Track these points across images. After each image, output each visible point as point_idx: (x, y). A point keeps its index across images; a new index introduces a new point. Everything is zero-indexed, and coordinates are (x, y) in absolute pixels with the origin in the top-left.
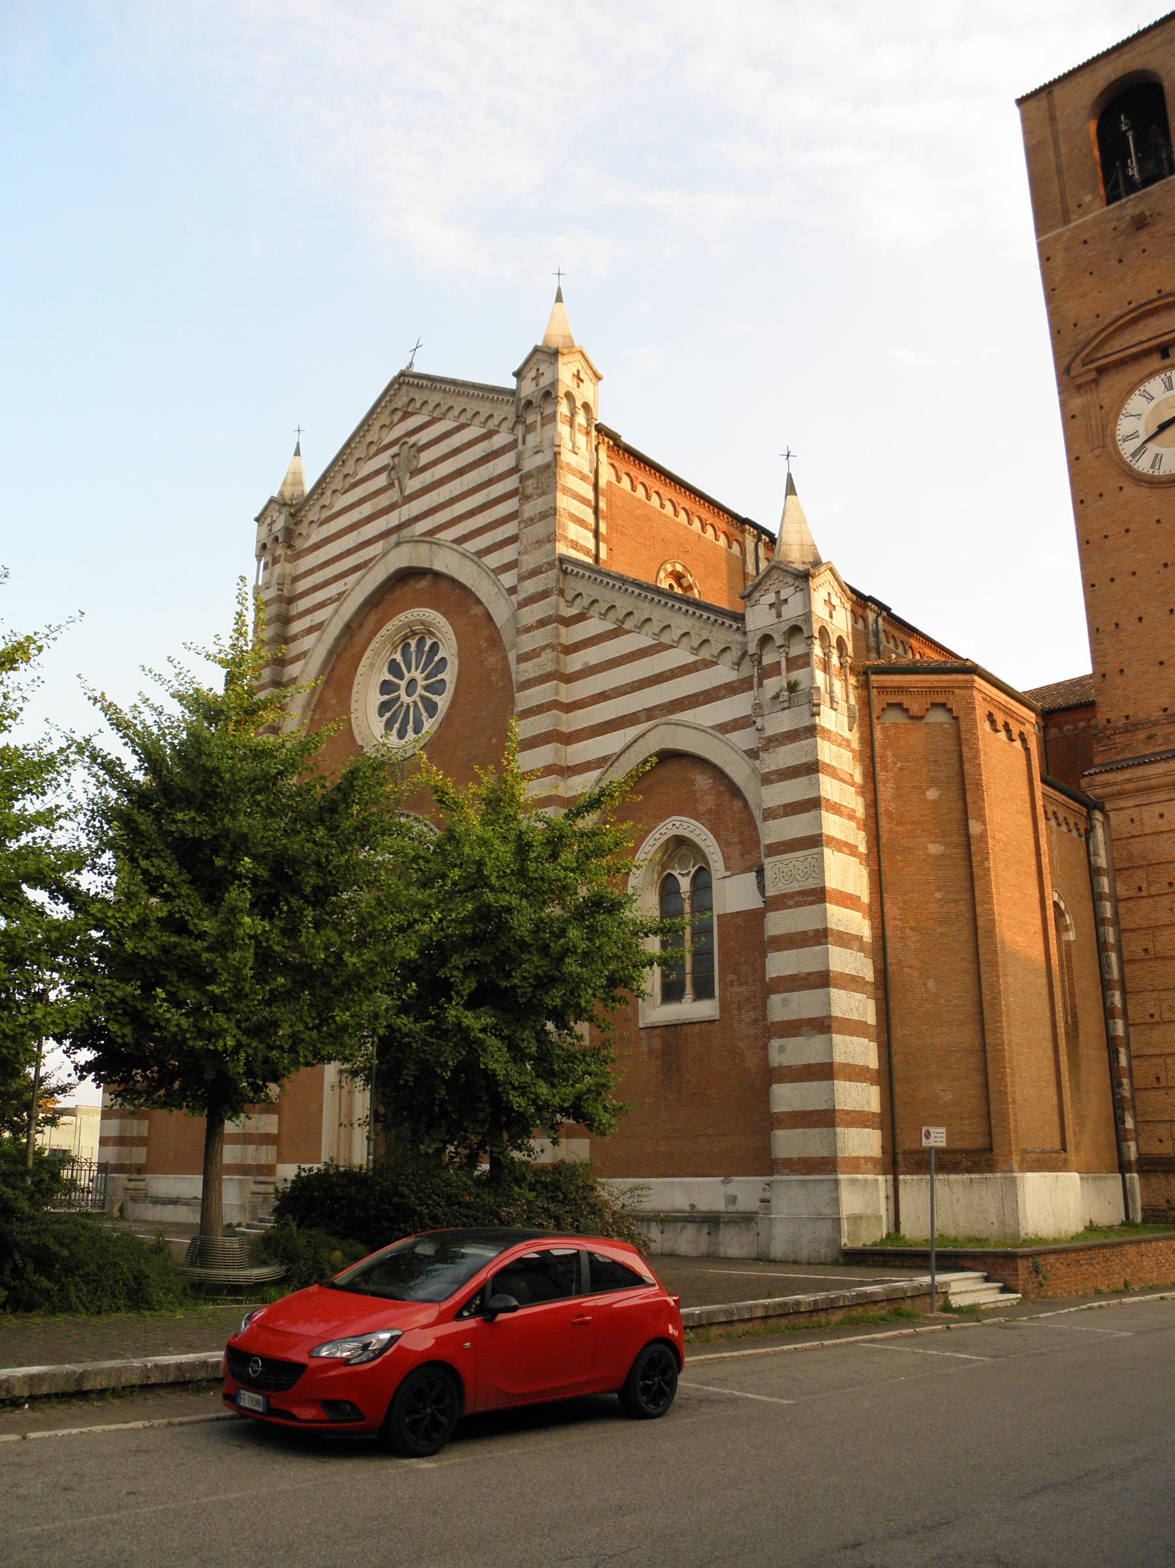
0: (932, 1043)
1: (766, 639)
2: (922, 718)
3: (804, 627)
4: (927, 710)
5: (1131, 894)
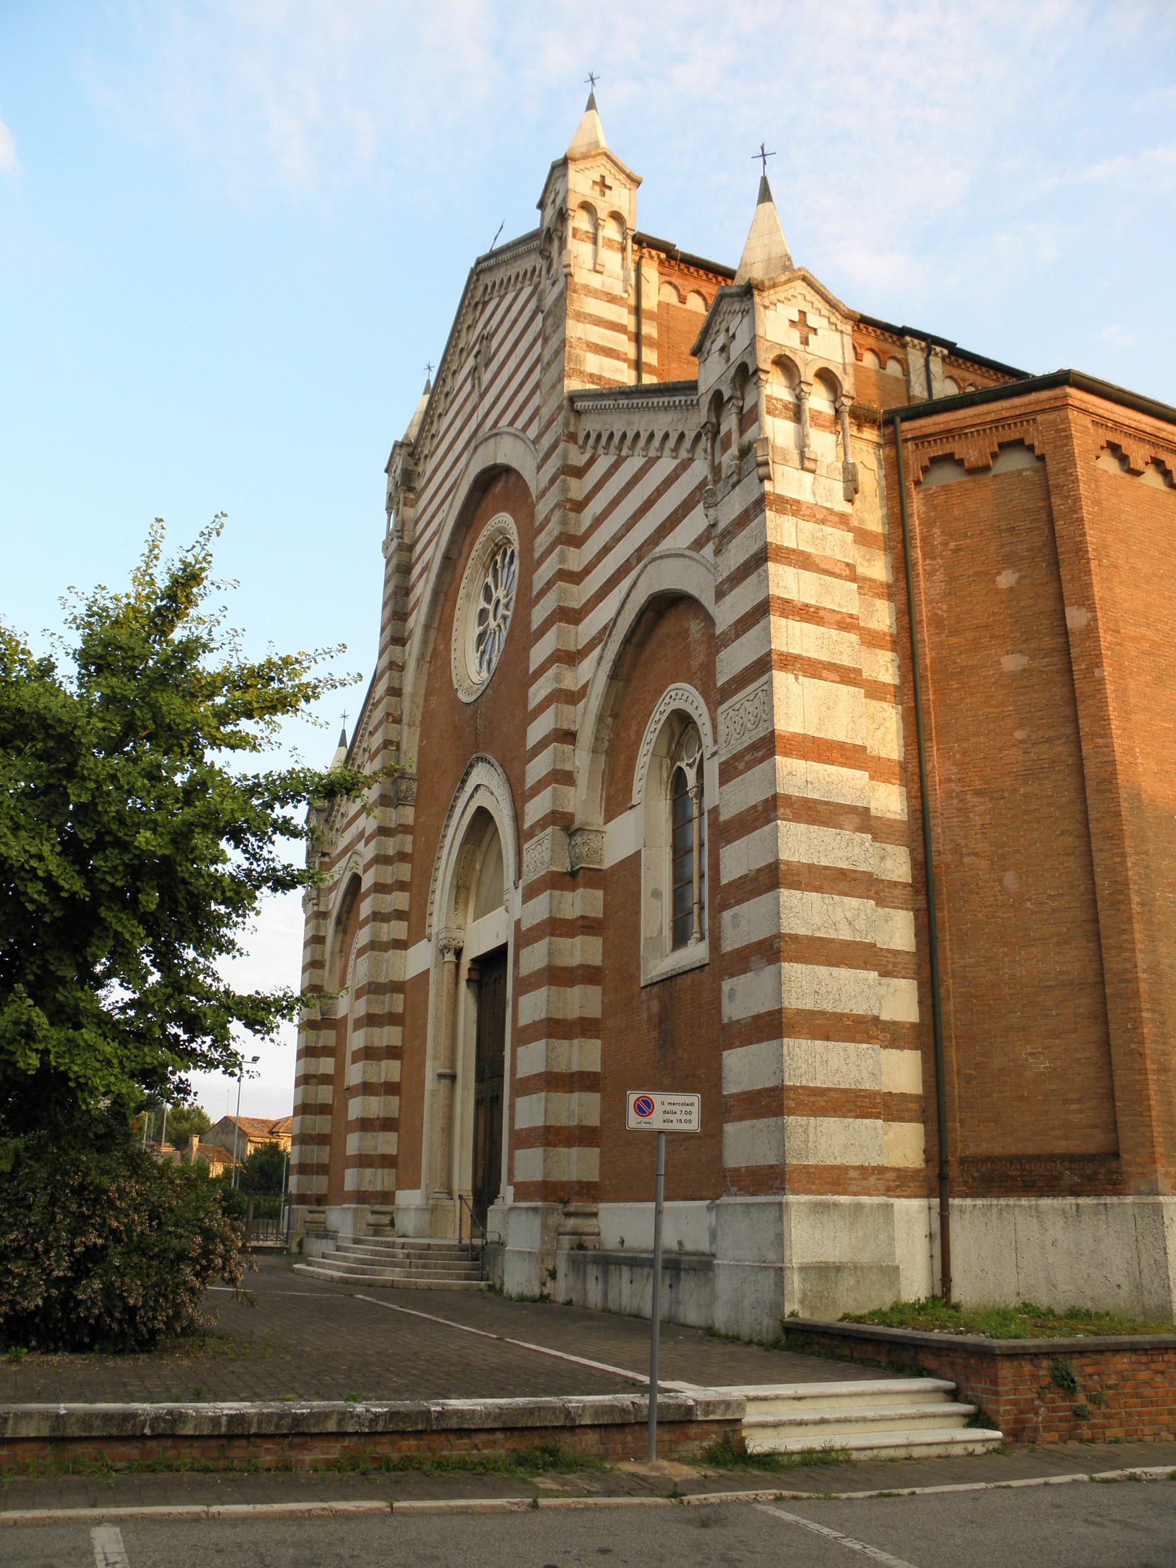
0: (1013, 977)
2: (986, 469)
4: (994, 456)
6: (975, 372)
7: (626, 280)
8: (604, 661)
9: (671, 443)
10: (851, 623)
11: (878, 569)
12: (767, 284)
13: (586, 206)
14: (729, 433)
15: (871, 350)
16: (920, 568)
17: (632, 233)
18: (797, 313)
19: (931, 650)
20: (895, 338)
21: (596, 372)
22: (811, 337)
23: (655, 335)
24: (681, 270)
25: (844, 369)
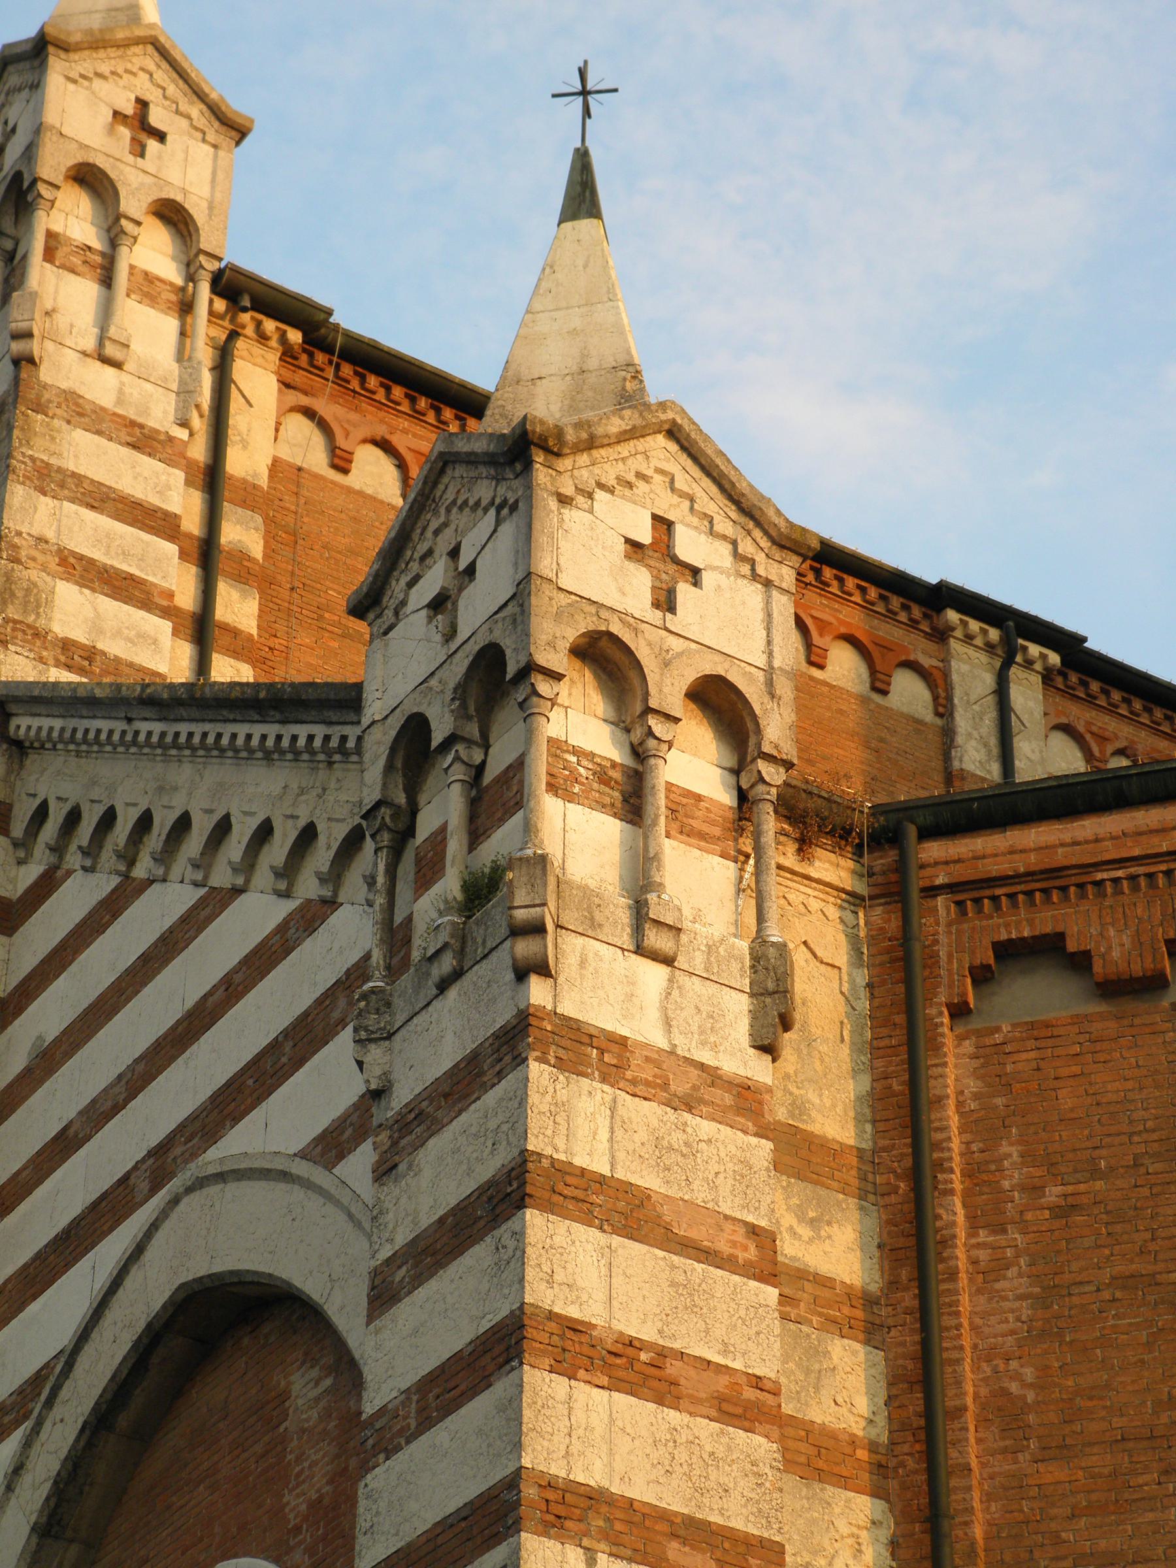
6: (1132, 719)
7: (185, 392)
8: (27, 1479)
9: (277, 851)
10: (758, 1405)
11: (839, 1248)
12: (570, 436)
13: (90, 178)
14: (440, 837)
15: (851, 640)
16: (961, 1253)
17: (214, 266)
18: (648, 521)
19: (988, 1497)
20: (917, 612)
21: (79, 635)
22: (684, 590)
23: (256, 549)
24: (340, 380)
25: (770, 683)
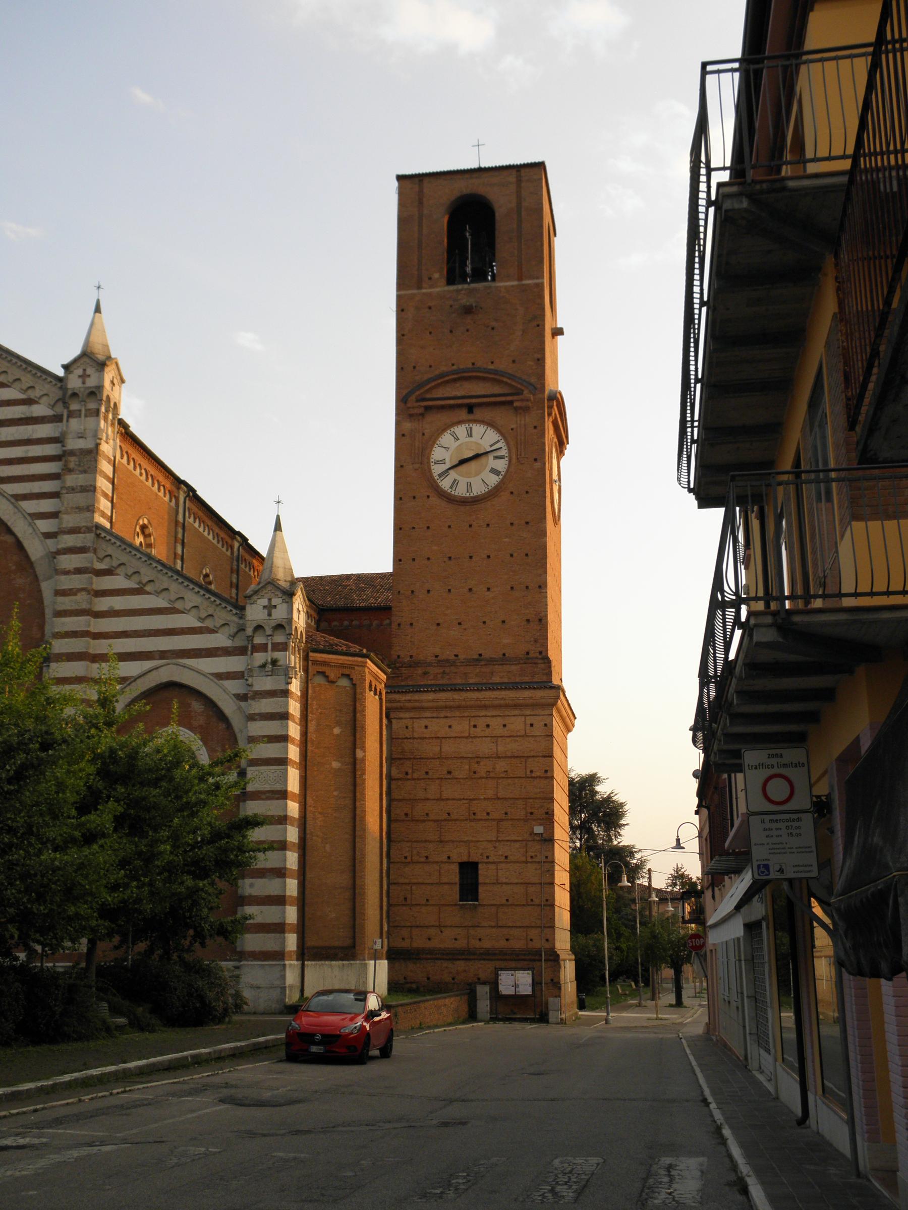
1: (259, 628)
3: (286, 625)
5: (401, 776)
